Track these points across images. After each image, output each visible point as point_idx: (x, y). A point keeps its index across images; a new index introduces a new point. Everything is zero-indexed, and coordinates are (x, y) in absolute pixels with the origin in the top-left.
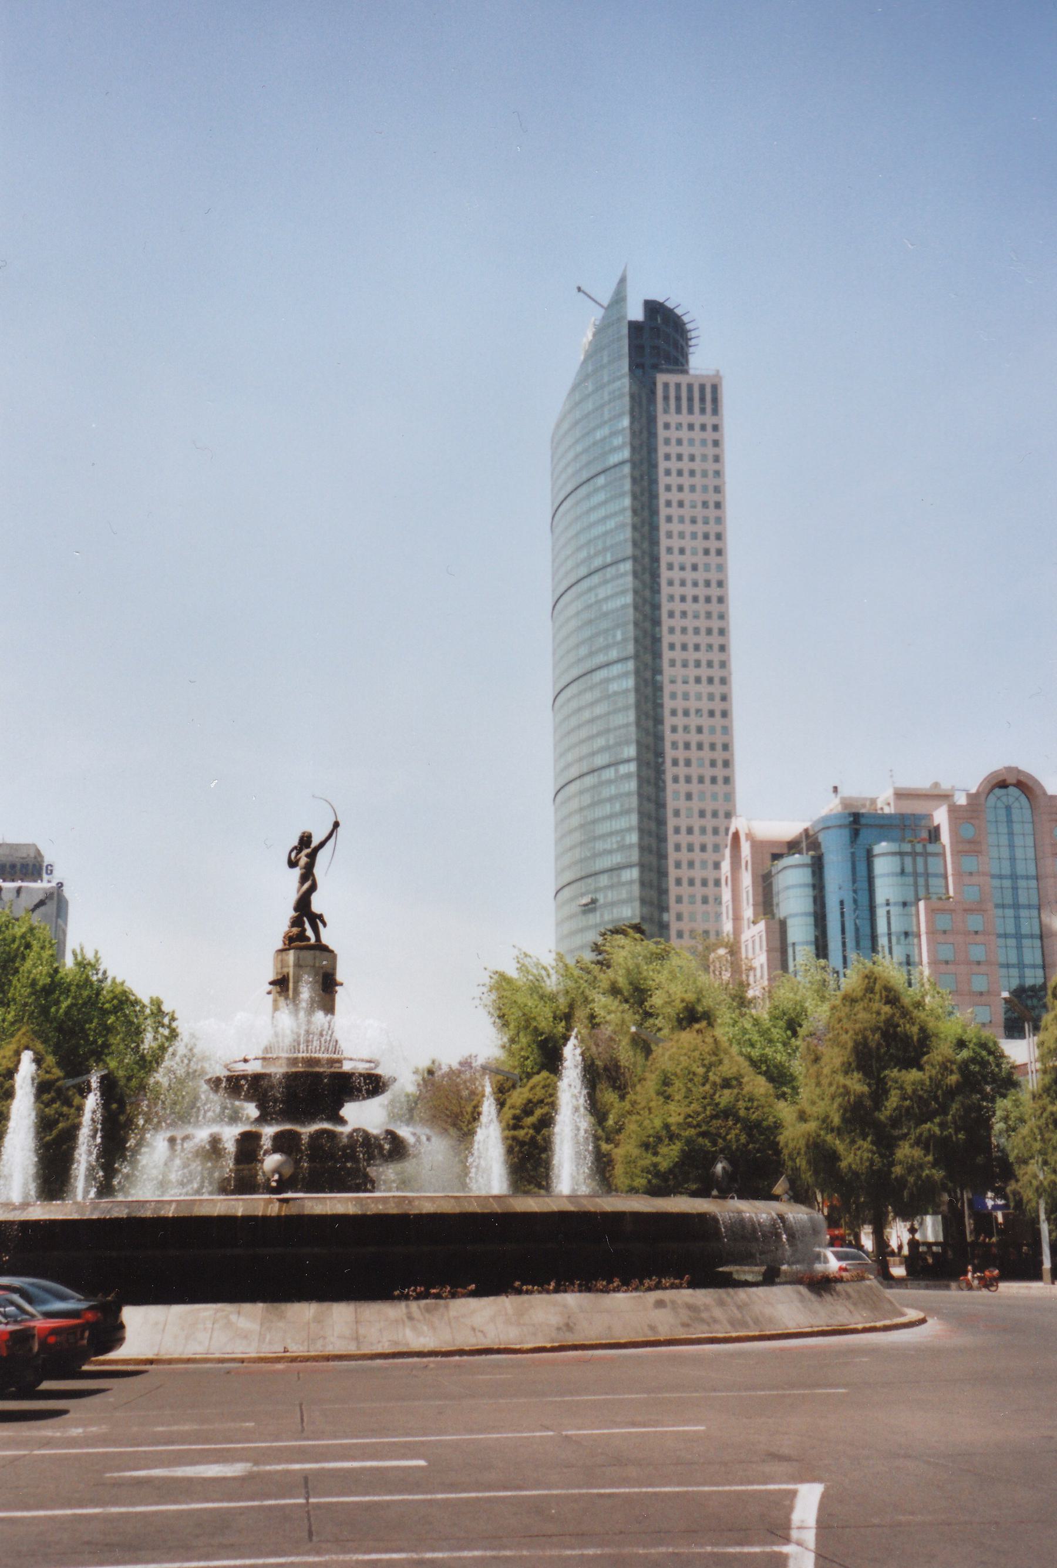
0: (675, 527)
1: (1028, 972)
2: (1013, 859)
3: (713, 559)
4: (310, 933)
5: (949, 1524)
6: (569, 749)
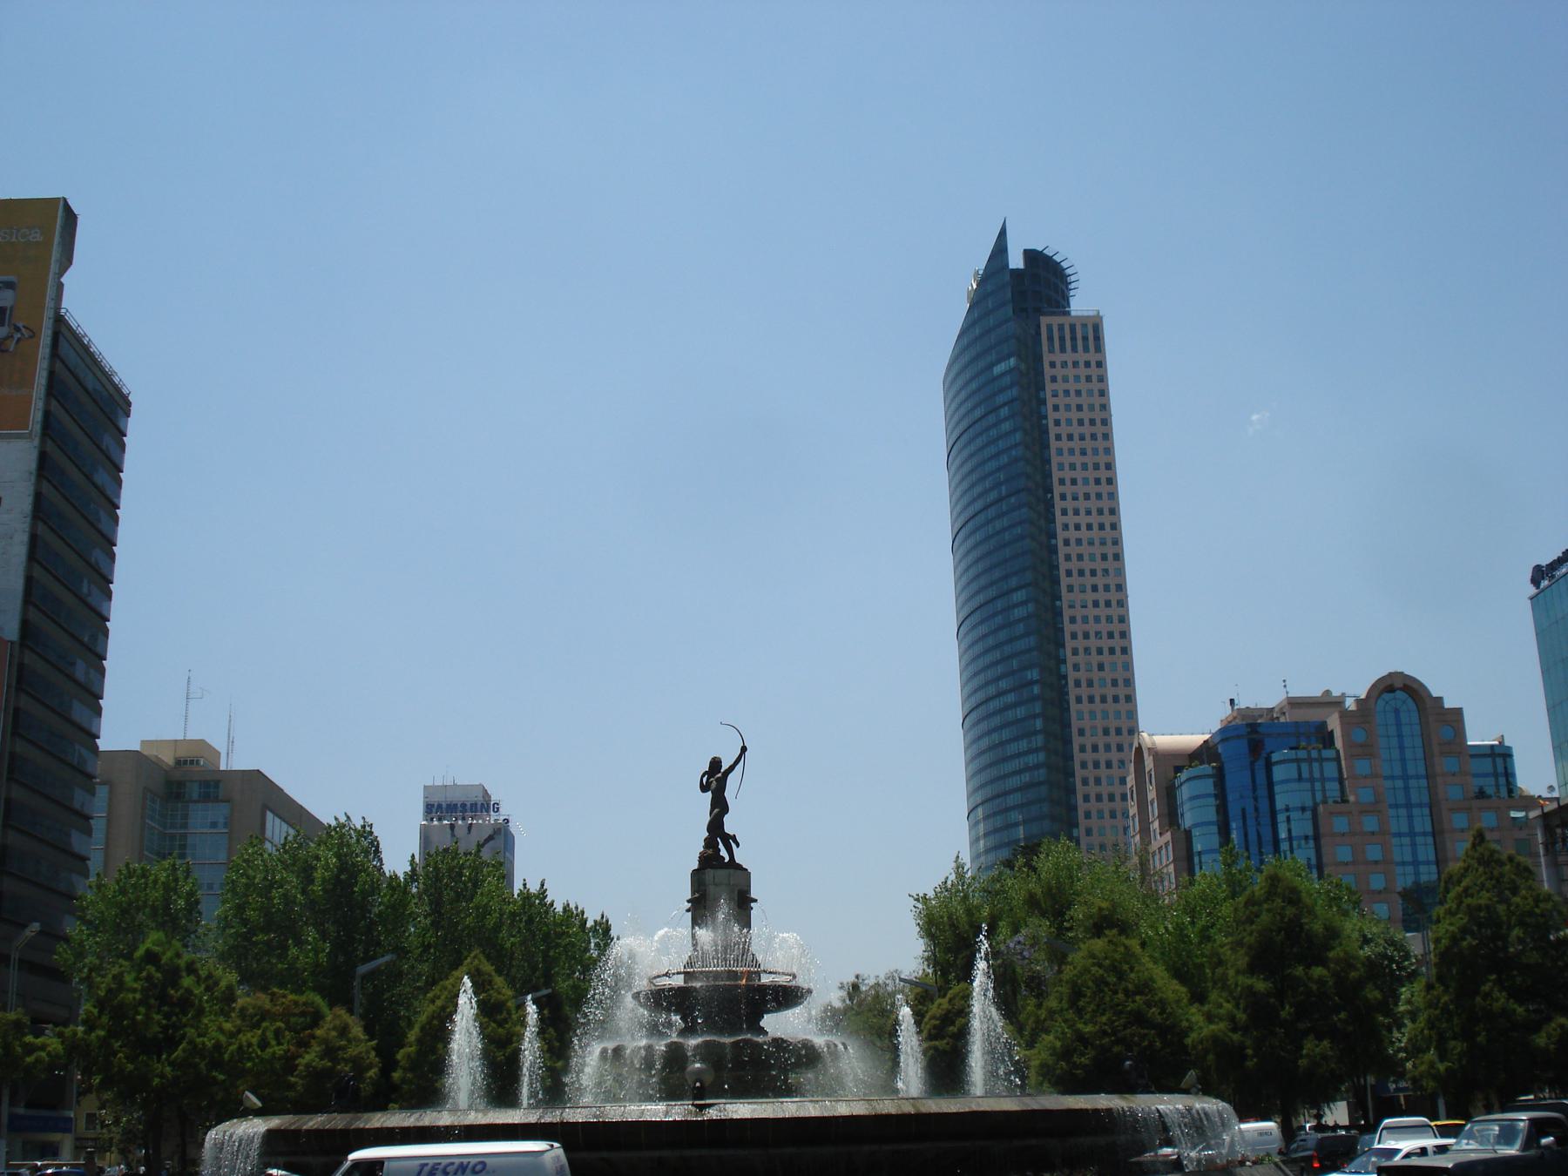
0: (1062, 415)
1: (1422, 869)
2: (1403, 760)
3: (1104, 489)
4: (724, 853)
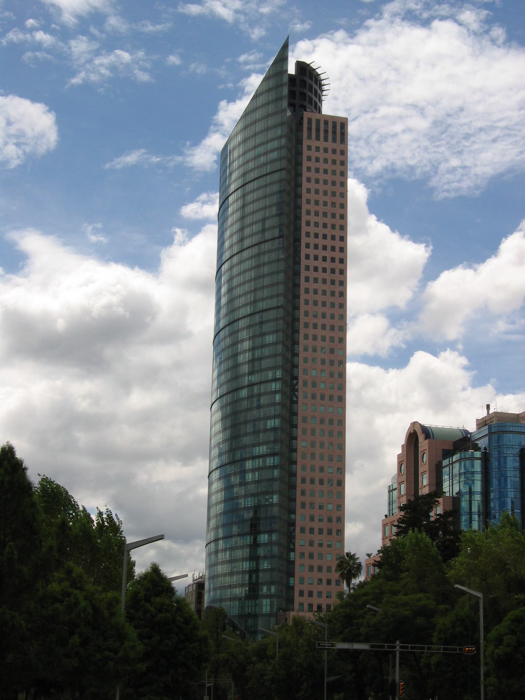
3: (338, 168)
5: (499, 447)
6: (249, 150)
